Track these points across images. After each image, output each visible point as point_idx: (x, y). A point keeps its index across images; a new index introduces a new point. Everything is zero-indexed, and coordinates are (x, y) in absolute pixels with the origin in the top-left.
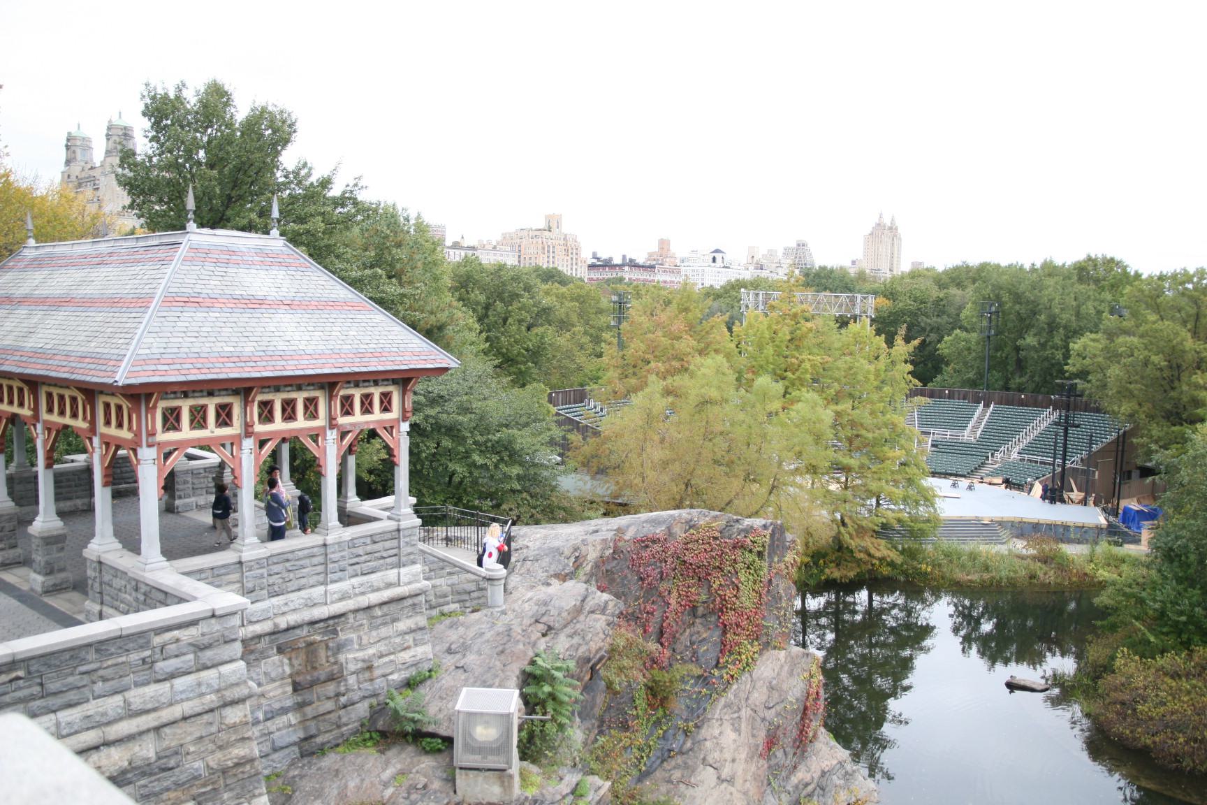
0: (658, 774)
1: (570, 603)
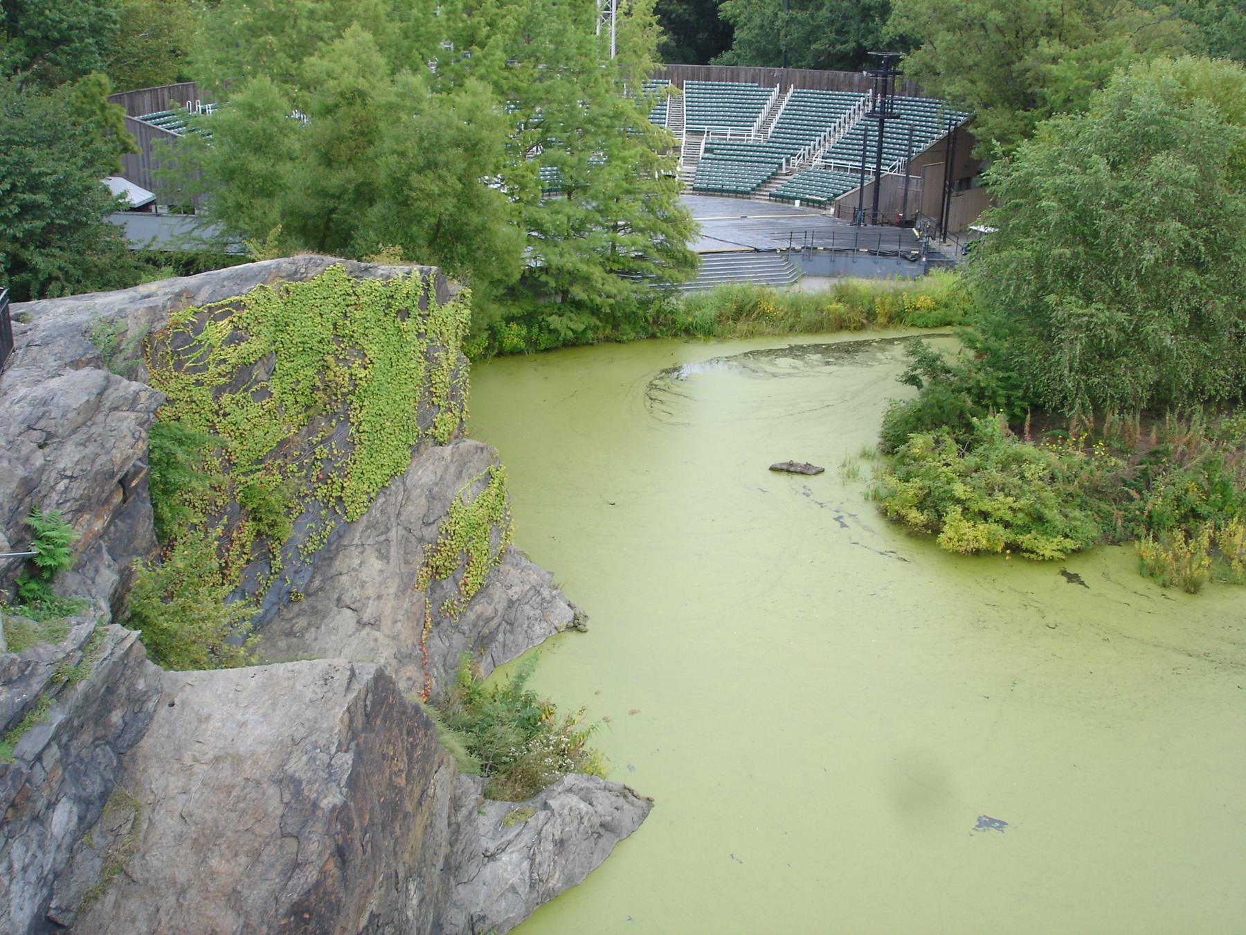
0: (276, 626)
1: (78, 399)
